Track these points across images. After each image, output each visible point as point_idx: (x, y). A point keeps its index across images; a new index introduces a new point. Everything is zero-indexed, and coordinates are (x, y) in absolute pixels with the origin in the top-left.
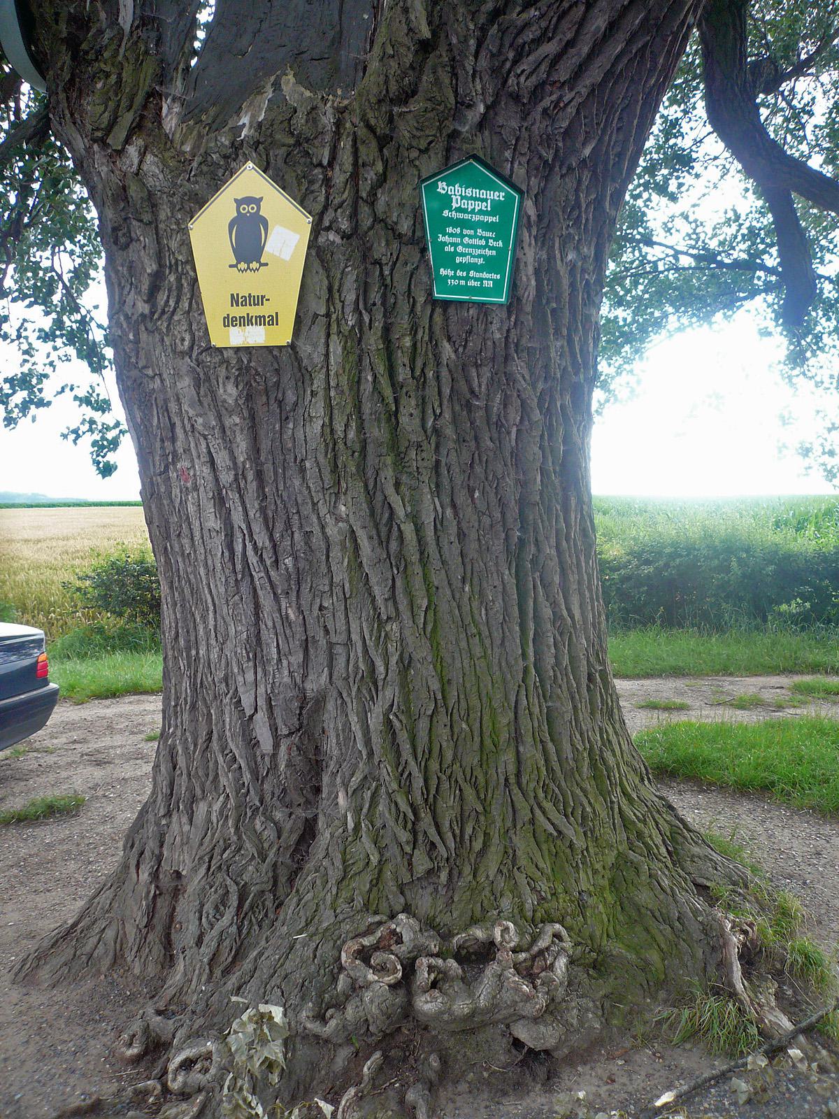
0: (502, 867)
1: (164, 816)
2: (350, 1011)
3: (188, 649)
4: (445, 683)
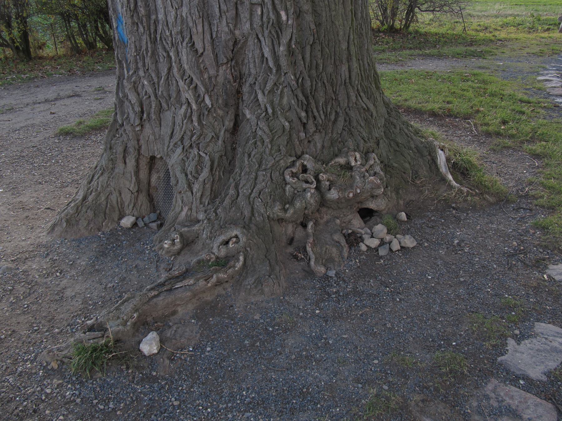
0: (344, 128)
1: (138, 125)
2: (298, 204)
3: (148, 16)
4: (318, 25)
